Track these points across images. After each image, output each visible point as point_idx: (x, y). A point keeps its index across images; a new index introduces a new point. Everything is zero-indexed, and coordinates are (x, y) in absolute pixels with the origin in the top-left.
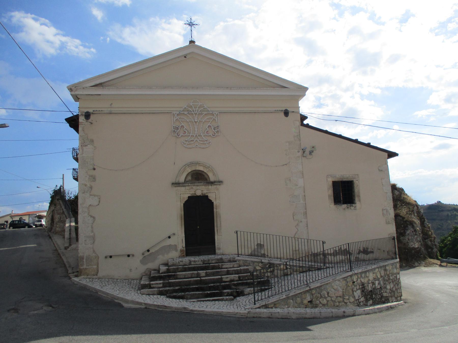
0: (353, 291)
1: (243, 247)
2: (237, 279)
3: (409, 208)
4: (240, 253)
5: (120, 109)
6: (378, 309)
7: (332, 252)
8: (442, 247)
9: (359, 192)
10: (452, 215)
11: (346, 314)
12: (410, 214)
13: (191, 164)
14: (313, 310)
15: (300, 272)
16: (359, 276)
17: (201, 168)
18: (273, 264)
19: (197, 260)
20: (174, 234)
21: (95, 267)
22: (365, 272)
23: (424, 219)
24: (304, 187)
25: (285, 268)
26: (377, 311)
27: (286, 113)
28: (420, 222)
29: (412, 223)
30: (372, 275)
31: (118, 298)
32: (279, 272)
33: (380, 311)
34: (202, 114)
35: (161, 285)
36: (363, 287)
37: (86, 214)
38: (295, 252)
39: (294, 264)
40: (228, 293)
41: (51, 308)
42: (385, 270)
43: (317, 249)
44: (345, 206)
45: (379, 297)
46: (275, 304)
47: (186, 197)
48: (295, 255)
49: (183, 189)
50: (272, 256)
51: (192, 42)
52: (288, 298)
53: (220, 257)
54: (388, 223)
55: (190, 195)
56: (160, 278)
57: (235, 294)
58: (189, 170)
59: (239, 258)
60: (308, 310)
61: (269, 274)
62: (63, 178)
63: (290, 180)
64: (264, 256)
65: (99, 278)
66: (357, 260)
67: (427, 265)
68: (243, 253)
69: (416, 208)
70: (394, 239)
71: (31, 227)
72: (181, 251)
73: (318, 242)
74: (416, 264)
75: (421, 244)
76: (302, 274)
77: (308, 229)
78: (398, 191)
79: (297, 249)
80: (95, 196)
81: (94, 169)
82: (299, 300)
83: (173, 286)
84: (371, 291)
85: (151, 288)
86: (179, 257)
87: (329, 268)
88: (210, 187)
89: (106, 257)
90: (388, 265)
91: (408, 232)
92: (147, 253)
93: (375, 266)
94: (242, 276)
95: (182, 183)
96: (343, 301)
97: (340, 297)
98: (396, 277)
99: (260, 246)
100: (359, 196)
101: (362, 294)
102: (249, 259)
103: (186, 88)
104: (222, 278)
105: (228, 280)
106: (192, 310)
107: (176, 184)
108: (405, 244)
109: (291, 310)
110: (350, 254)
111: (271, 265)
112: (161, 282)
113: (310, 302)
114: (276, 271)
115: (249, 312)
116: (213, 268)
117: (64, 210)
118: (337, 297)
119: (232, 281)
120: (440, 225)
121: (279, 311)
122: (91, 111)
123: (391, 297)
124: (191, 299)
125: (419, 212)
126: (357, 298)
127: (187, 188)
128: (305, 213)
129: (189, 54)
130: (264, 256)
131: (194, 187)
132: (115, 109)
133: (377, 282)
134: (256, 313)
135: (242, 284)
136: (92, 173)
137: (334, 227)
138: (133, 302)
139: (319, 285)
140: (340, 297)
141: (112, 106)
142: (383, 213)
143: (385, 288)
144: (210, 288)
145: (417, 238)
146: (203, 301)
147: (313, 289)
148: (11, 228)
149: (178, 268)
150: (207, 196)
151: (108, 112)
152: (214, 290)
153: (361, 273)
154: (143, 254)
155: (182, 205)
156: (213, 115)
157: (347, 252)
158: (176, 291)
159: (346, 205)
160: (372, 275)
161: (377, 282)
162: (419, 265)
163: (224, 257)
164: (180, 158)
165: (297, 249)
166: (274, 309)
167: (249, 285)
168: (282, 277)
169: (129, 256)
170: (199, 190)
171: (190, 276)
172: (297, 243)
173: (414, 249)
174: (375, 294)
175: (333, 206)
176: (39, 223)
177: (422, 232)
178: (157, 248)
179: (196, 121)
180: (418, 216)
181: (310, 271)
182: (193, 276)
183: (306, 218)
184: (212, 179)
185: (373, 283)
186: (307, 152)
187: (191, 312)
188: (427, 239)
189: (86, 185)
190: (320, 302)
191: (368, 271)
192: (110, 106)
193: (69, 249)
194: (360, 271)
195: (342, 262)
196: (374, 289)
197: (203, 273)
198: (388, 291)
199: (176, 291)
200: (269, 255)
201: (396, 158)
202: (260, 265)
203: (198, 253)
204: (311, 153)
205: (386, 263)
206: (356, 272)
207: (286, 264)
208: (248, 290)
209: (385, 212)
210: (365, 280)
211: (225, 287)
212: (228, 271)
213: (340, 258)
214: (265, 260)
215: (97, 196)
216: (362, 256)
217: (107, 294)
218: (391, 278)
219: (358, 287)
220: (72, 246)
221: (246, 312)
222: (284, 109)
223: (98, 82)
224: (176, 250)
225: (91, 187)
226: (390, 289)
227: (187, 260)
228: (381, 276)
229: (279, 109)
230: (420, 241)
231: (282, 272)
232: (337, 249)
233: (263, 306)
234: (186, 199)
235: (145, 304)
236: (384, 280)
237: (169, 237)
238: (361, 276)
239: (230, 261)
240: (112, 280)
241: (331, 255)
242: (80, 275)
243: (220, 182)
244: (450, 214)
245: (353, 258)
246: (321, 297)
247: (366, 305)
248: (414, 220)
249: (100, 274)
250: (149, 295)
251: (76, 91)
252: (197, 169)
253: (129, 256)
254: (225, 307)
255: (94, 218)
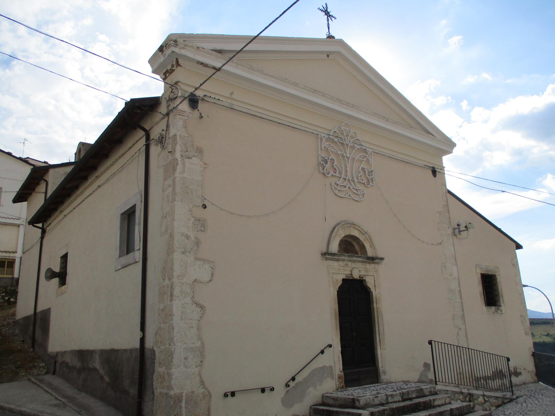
5: (246, 106)
17: (356, 233)
24: (459, 278)
37: (188, 300)
49: (335, 264)
77: (467, 340)
80: (204, 261)
81: (205, 207)
92: (292, 384)
100: (502, 296)
127: (341, 263)
128: (463, 317)
141: (233, 96)
151: (227, 105)
164: (323, 213)
170: (357, 269)
175: (484, 308)
179: (348, 156)
184: (370, 253)
189: (188, 237)
192: (229, 96)
223: (219, 47)
225: (198, 243)
234: (340, 283)
243: (382, 259)
251: (183, 48)
255: (202, 307)
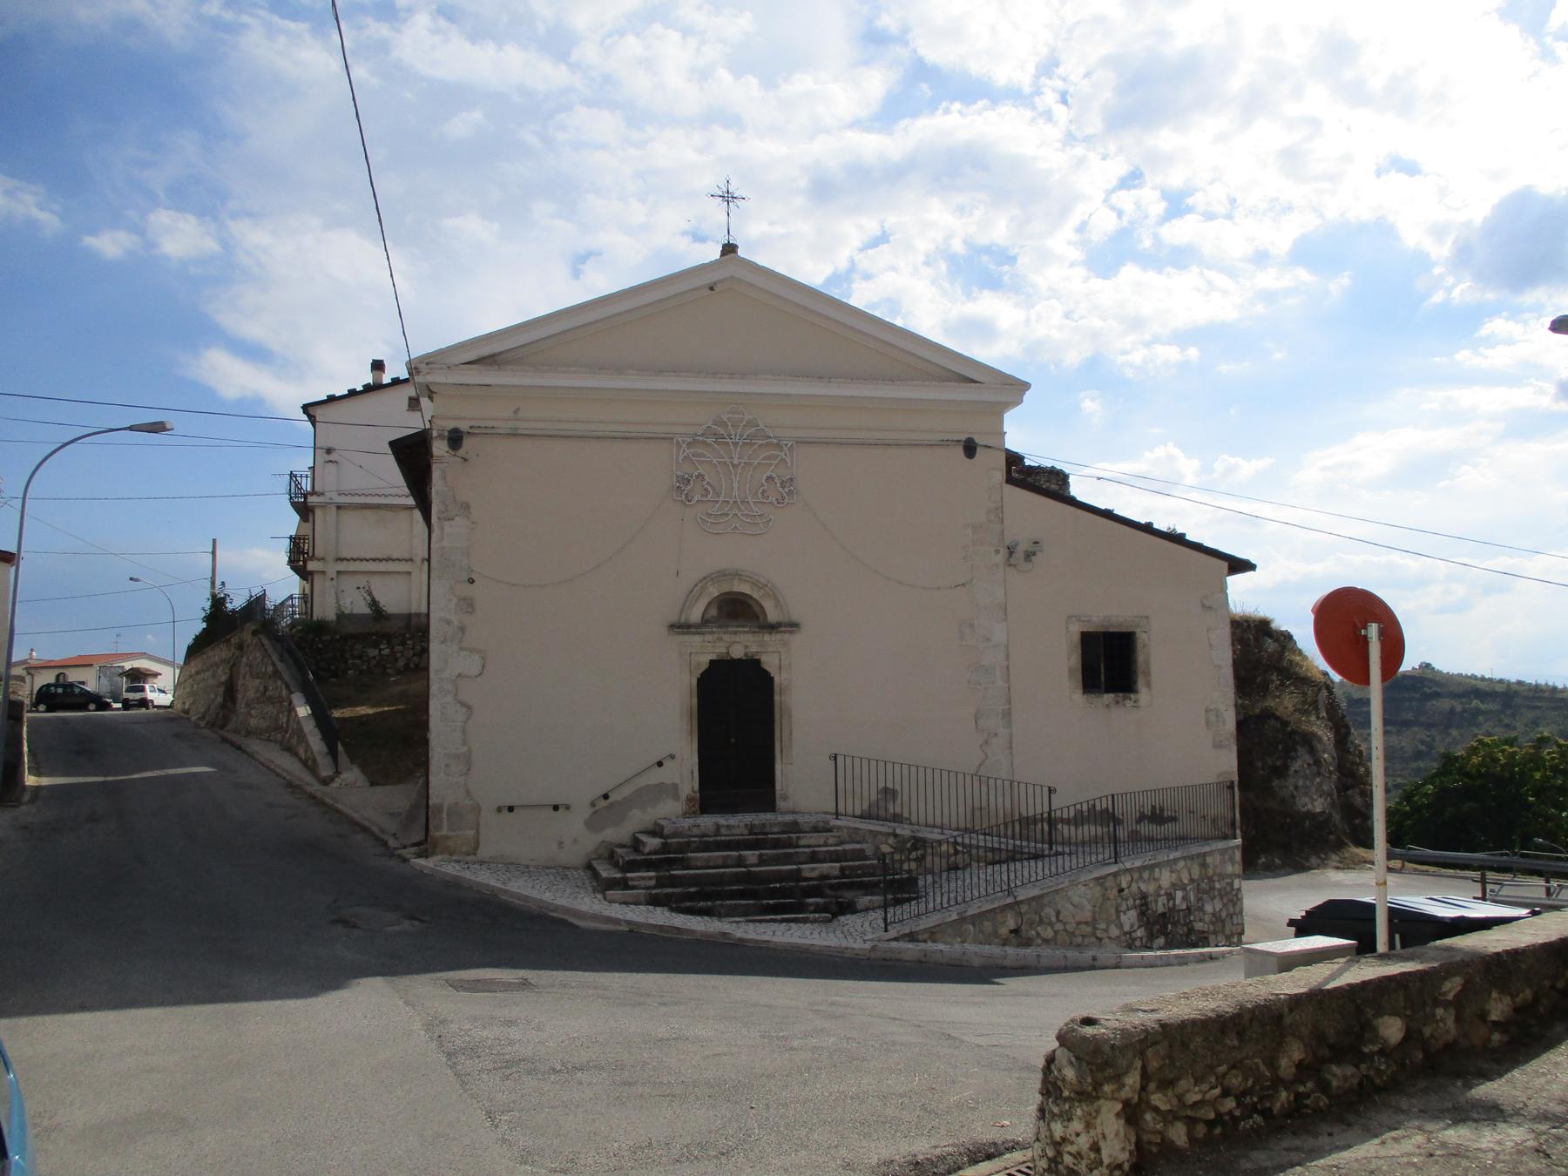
0: (1118, 912)
1: (849, 795)
2: (837, 872)
3: (1304, 694)
4: (841, 809)
6: (1177, 956)
7: (1072, 814)
8: (1406, 813)
9: (1148, 664)
10: (1464, 711)
11: (1098, 964)
12: (1306, 713)
13: (721, 575)
14: (1023, 951)
15: (988, 864)
16: (1136, 876)
17: (745, 588)
18: (924, 840)
19: (737, 823)
20: (672, 757)
21: (472, 832)
22: (1152, 867)
23: (1347, 727)
25: (951, 851)
26: (1172, 960)
27: (970, 449)
28: (1336, 735)
29: (1309, 741)
30: (1167, 875)
31: (557, 908)
32: (937, 859)
33: (1182, 961)
34: (752, 444)
35: (653, 883)
36: (1144, 902)
37: (449, 698)
38: (977, 813)
39: (974, 842)
40: (817, 905)
41: (416, 923)
42: (1204, 865)
43: (1034, 806)
44: (1108, 698)
45: (1182, 930)
46: (932, 933)
47: (704, 660)
48: (977, 821)
50: (922, 821)
51: (729, 249)
52: (962, 920)
53: (788, 818)
54: (1218, 745)
55: (714, 657)
56: (648, 865)
57: (834, 908)
58: (714, 591)
59: (838, 823)
60: (1010, 950)
61: (913, 865)
62: (214, 553)
63: (972, 625)
64: (897, 818)
65: (482, 863)
66: (1135, 838)
67: (1344, 866)
68: (850, 811)
69: (1325, 693)
70: (1231, 787)
71: (106, 706)
72: (689, 800)
73: (1038, 789)
74: (1314, 860)
75: (1333, 804)
76: (997, 867)
78: (1276, 640)
79: (984, 803)
80: (472, 650)
81: (471, 581)
82: (987, 925)
83: (681, 885)
84: (1164, 915)
85: (627, 887)
86: (685, 815)
87: (1063, 854)
88: (767, 637)
89: (499, 810)
90: (1211, 853)
91: (1296, 766)
92: (603, 803)
93: (1177, 854)
94: (850, 867)
95: (696, 626)
96: (1094, 935)
97: (1086, 923)
98: (1231, 884)
99: (889, 793)
100: (1147, 673)
101: (1139, 920)
102: (863, 826)
103: (714, 373)
104: (799, 871)
105: (815, 874)
106: (741, 940)
107: (680, 627)
108: (1283, 801)
109: (971, 947)
110: (1117, 821)
111: (919, 843)
112: (652, 874)
113: (1015, 932)
114: (929, 858)
115: (874, 948)
116: (776, 844)
117: (280, 666)
118: (1079, 923)
119: (823, 877)
120: (1422, 742)
121: (942, 949)
122: (463, 426)
123: (1215, 933)
124: (728, 915)
125: (1332, 707)
126: (1127, 928)
127: (709, 637)
128: (1007, 715)
129: (722, 281)
130: (897, 818)
131: (726, 637)
132: (526, 425)
133: (1179, 894)
134: (891, 950)
135: (850, 886)
136: (467, 590)
137: (1077, 752)
138: (596, 917)
139: (1035, 892)
140: (1086, 923)
142: (1207, 722)
143: (1201, 909)
144: (773, 893)
145: (1321, 784)
146: (760, 921)
147: (1022, 902)
148: (42, 707)
149: (689, 843)
150: (758, 661)
152: (786, 898)
153: (1142, 869)
154: (593, 805)
155: (695, 682)
156: (778, 446)
157: (1108, 817)
158: (690, 897)
159: (1111, 696)
160: (1167, 875)
161: (1179, 894)
162: (1323, 865)
163: (800, 819)
165: (984, 803)
166: (930, 944)
167: (868, 888)
168: (944, 875)
169: (556, 808)
170: (739, 643)
171: (720, 862)
172: (984, 789)
173: (1310, 815)
174: (1174, 924)
175: (1079, 696)
176: (138, 696)
177: (1340, 768)
178: (627, 791)
180: (1330, 719)
181: (1014, 860)
182: (729, 862)
183: (1009, 724)
184: (773, 615)
185: (1170, 897)
186: (1019, 553)
187: (741, 943)
188: (1352, 787)
189: (449, 622)
190: (1038, 934)
191: (1158, 865)
193: (335, 785)
194: (1138, 863)
195: (1095, 841)
196: (1173, 910)
197: (751, 856)
198: (1207, 918)
199: (690, 897)
200: (914, 819)
201: (1250, 574)
202: (891, 840)
203: (732, 808)
204: (1029, 556)
205: (1207, 849)
206: (1128, 865)
207: (956, 843)
208: (864, 900)
209: (1212, 718)
210: (1150, 888)
211: (810, 892)
212: (814, 853)
213: (1089, 830)
214: (904, 831)
215: (479, 651)
216: (1146, 829)
217: (526, 898)
218: (1217, 885)
219: (1131, 902)
220: (344, 776)
221: (868, 946)
222: (964, 437)
223: (486, 351)
224: (676, 797)
225: (462, 629)
226: (1214, 914)
227: (707, 822)
228: (1192, 880)
229: (951, 437)
230: (1330, 795)
231: (944, 861)
232: (1085, 808)
233: (904, 935)
234: (704, 667)
235: (628, 922)
236: (1198, 890)
237: (660, 764)
238: (1141, 877)
239: (816, 829)
240: (511, 865)
241: (1068, 822)
242: (433, 854)
243: (793, 626)
244: (1459, 708)
245: (1122, 833)
246: (1041, 922)
247: (1150, 948)
248: (1315, 729)
249: (484, 852)
250: (625, 903)
252: (736, 589)
253: (556, 808)
254: (815, 934)
255: (469, 708)
